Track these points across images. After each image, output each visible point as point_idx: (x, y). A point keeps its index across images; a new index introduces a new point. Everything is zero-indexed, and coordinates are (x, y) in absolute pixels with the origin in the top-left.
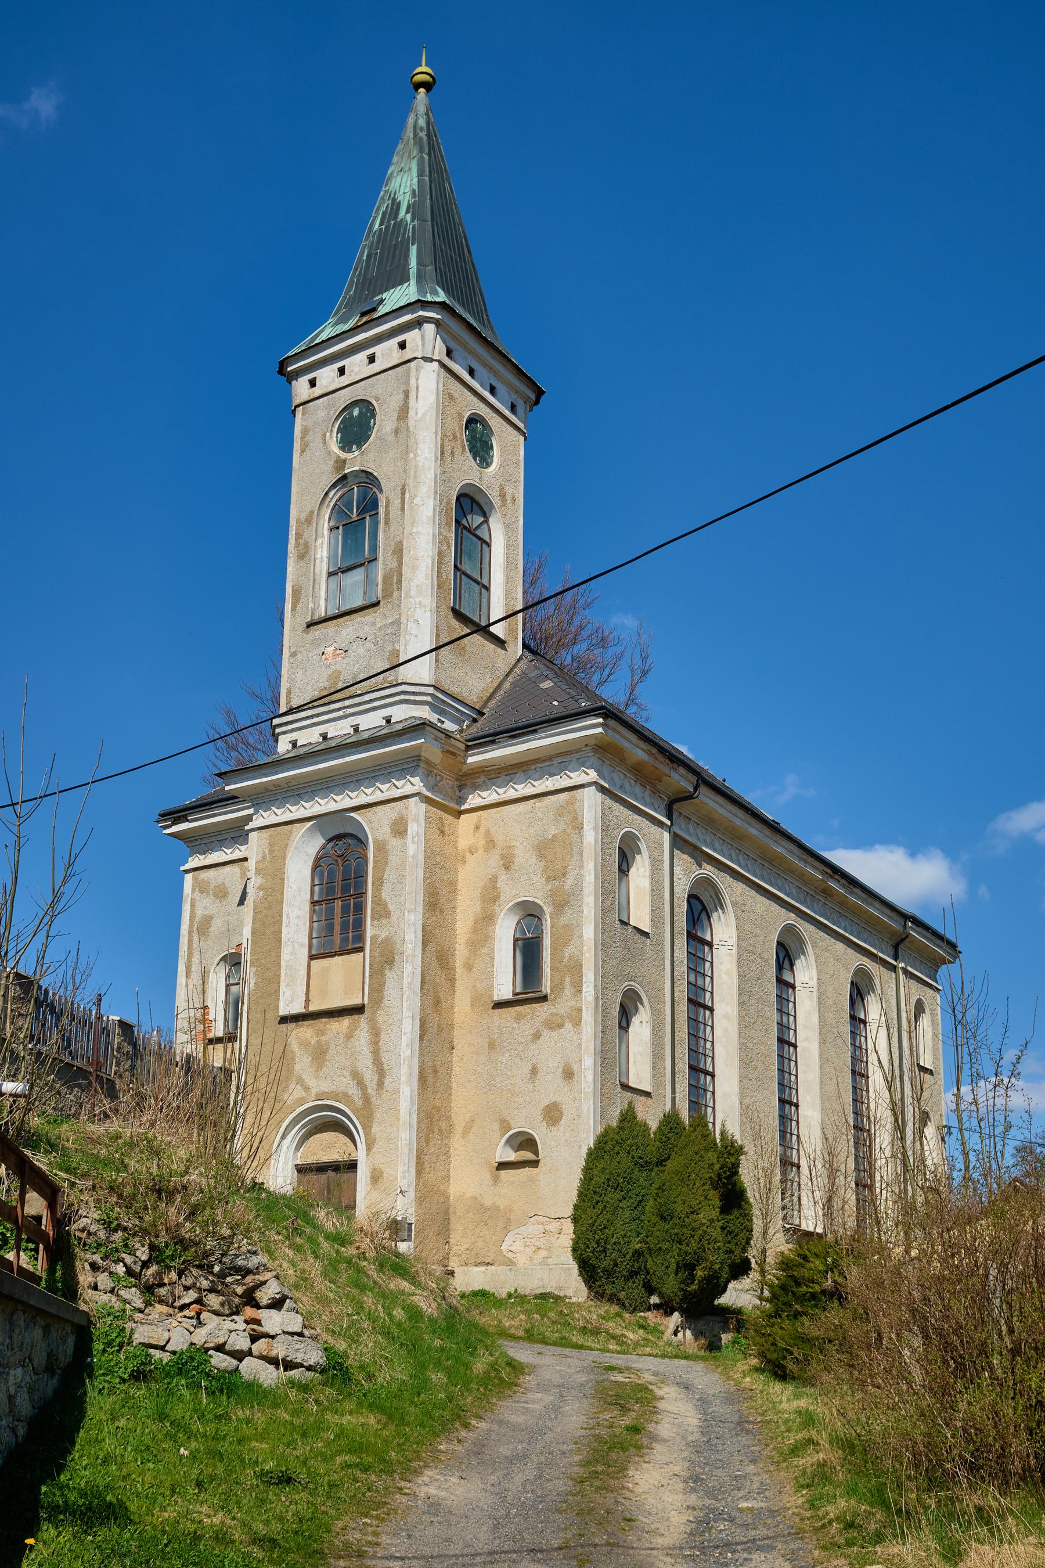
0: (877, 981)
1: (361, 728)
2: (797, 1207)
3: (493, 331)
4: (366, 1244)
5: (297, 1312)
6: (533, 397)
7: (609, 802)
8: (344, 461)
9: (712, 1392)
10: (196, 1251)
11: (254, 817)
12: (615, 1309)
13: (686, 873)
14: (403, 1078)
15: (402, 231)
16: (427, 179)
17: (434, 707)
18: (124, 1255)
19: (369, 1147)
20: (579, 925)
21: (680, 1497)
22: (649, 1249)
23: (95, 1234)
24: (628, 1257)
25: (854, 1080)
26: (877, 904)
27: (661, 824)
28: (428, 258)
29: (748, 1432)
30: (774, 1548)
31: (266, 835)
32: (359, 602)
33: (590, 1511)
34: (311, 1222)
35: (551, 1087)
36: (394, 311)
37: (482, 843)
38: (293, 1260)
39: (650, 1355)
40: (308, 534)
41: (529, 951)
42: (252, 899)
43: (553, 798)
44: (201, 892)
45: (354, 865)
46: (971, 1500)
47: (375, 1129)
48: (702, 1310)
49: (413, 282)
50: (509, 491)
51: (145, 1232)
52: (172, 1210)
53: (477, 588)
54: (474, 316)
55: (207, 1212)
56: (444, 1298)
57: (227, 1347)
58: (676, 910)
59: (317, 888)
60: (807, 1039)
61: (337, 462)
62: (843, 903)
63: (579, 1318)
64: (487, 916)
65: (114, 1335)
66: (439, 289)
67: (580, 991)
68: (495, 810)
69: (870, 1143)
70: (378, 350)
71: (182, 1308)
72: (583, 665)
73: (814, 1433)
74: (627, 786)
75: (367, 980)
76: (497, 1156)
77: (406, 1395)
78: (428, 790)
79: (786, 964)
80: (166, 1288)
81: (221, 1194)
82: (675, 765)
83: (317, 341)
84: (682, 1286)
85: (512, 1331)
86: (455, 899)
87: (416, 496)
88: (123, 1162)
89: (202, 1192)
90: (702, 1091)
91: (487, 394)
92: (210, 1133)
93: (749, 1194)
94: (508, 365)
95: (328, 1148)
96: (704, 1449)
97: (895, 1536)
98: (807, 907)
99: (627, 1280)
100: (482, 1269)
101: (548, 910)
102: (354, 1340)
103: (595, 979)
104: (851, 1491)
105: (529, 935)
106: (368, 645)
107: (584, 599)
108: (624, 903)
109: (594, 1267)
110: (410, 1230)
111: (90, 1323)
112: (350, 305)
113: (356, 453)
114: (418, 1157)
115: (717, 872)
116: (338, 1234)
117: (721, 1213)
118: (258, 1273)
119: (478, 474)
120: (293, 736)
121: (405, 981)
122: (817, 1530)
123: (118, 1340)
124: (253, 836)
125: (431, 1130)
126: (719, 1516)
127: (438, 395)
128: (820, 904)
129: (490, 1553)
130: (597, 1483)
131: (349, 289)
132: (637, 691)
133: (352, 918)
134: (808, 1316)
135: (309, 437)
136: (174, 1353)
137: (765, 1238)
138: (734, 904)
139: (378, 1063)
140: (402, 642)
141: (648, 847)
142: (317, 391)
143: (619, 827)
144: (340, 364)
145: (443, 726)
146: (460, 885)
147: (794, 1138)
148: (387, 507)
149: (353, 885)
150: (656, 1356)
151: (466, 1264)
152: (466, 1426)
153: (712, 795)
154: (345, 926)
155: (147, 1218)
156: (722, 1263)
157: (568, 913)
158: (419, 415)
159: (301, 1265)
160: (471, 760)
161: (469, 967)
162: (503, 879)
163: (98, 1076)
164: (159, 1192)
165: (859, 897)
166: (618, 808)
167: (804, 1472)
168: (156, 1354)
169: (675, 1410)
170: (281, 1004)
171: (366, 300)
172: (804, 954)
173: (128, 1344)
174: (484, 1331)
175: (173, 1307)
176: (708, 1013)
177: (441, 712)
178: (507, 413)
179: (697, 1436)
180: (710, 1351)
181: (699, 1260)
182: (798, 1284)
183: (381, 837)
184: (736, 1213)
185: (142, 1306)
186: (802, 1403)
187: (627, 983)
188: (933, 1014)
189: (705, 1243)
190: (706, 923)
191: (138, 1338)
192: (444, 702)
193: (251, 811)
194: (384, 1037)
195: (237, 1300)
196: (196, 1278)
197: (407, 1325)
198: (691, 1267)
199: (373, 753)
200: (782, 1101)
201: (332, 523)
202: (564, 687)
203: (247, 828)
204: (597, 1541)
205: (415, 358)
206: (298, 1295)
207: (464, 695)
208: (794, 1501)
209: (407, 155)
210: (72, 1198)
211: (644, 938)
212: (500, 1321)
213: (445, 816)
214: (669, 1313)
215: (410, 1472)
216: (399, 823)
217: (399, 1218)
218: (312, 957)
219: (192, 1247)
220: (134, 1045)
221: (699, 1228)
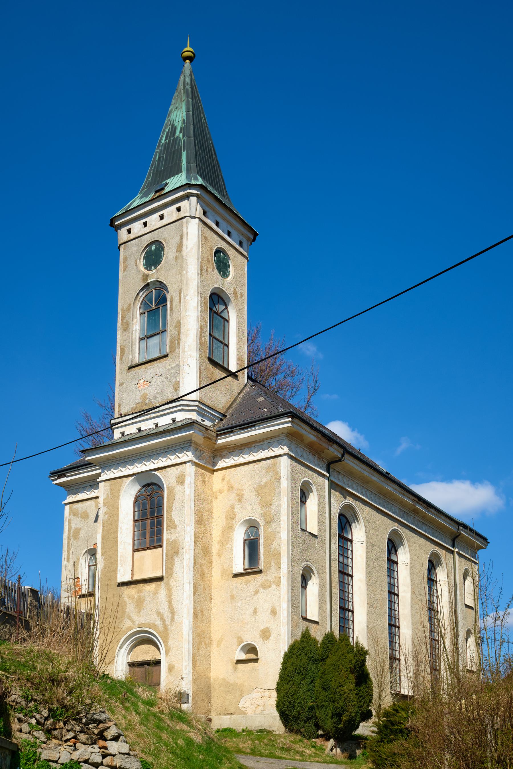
0: (443, 559)
1: (159, 425)
2: (396, 682)
3: (229, 201)
4: (164, 706)
5: (126, 743)
6: (252, 237)
7: (295, 464)
8: (147, 276)
10: (73, 712)
11: (102, 474)
12: (299, 737)
13: (338, 502)
15: (177, 143)
16: (191, 113)
17: (199, 413)
18: (35, 714)
19: (167, 652)
22: (317, 706)
23: (20, 703)
24: (306, 710)
26: (443, 517)
28: (193, 159)
32: (157, 355)
34: (133, 694)
35: (264, 620)
36: (173, 190)
37: (226, 487)
38: (124, 715)
39: (317, 762)
40: (128, 317)
41: (252, 546)
42: (101, 519)
43: (264, 462)
44: (74, 515)
47: (170, 643)
49: (184, 173)
50: (239, 291)
51: (46, 702)
52: (60, 691)
53: (222, 345)
54: (218, 191)
55: (78, 692)
56: (206, 733)
57: (90, 761)
58: (332, 523)
61: (143, 276)
62: (424, 517)
63: (280, 743)
64: (229, 528)
65: (31, 755)
66: (199, 177)
67: (280, 568)
68: (233, 469)
69: (439, 646)
70: (165, 212)
71: (66, 741)
72: (281, 387)
74: (305, 455)
75: (164, 563)
78: (196, 459)
79: (393, 551)
80: (57, 731)
81: (85, 682)
82: (331, 443)
83: (131, 207)
84: (335, 725)
85: (244, 750)
87: (187, 295)
88: (33, 665)
89: (75, 681)
90: (347, 621)
91: (226, 236)
92: (79, 648)
93: (371, 676)
94: (238, 220)
95: (145, 653)
98: (405, 520)
99: (305, 722)
100: (229, 717)
101: (262, 524)
102: (156, 756)
103: (288, 561)
105: (252, 537)
106: (162, 378)
109: (288, 715)
110: (188, 698)
111: (18, 749)
112: (149, 186)
113: (154, 271)
115: (354, 501)
116: (149, 700)
117: (356, 686)
118: (106, 723)
119: (221, 282)
121: (185, 563)
123: (33, 758)
124: (101, 484)
127: (198, 237)
128: (412, 517)
131: (148, 178)
132: (311, 401)
133: (156, 529)
135: (128, 262)
136: (62, 764)
137: (380, 699)
140: (181, 377)
141: (317, 488)
142: (132, 236)
143: (300, 477)
144: (144, 220)
145: (204, 423)
146: (214, 510)
147: (397, 645)
148: (171, 301)
149: (156, 511)
150: (320, 762)
151: (220, 714)
154: (152, 534)
155: (47, 695)
156: (356, 713)
157: (273, 526)
158: (189, 249)
159: (129, 717)
160: (219, 442)
161: (219, 555)
162: (237, 507)
163: (20, 618)
164: (53, 681)
165: (433, 514)
166: (300, 467)
168: (53, 765)
170: (119, 576)
171: (158, 183)
172: (403, 545)
173: (38, 760)
174: (227, 750)
175: (61, 740)
176: (350, 578)
177: (203, 415)
178: (238, 247)
180: (350, 759)
181: (344, 711)
182: (393, 725)
183: (171, 485)
184: (364, 686)
185: (45, 740)
187: (305, 563)
189: (347, 702)
190: (349, 529)
191: (43, 757)
192: (204, 410)
193: (100, 471)
194: (174, 593)
195: (95, 737)
196: (73, 725)
197: (185, 748)
198: (339, 715)
201: (142, 311)
202: (270, 401)
203: (98, 480)
205: (186, 217)
206: (126, 733)
207: (215, 406)
209: (179, 99)
210: (7, 685)
211: (314, 538)
212: (238, 745)
213: (206, 473)
214: (328, 739)
216: (181, 477)
217: (183, 691)
218: (135, 551)
219: (71, 709)
220: (39, 602)
221: (344, 694)
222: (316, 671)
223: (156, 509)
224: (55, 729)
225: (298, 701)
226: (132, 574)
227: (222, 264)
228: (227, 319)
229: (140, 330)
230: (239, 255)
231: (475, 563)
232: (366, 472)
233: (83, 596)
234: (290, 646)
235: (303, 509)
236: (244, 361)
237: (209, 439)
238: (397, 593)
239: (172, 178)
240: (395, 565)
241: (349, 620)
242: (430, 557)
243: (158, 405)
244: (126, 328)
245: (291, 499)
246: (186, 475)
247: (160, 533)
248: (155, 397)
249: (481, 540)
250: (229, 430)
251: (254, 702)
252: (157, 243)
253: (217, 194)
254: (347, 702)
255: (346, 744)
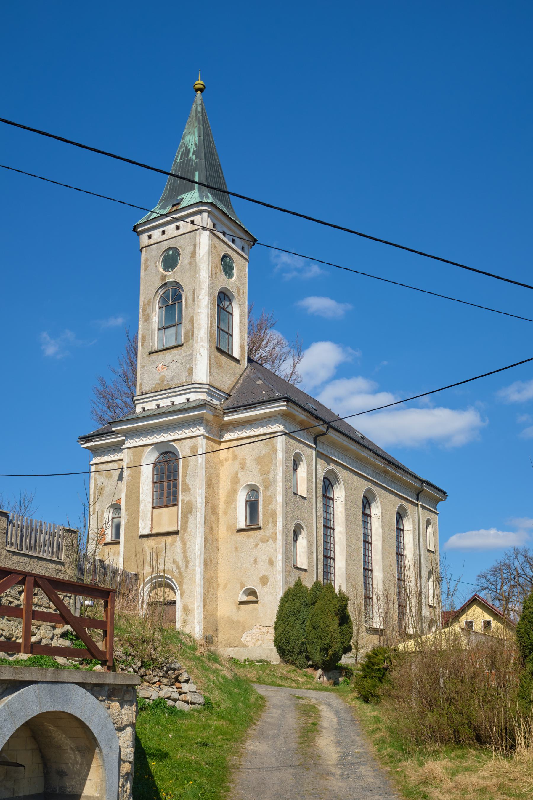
0: (409, 511)
8: (166, 276)
9: (340, 708)
11: (126, 442)
12: (293, 667)
13: (323, 468)
14: (197, 564)
15: (191, 164)
16: (202, 138)
17: (209, 394)
19: (182, 595)
20: (276, 496)
21: (334, 748)
22: (308, 642)
25: (398, 558)
26: (409, 476)
27: (311, 447)
29: (355, 724)
30: (367, 764)
31: (132, 451)
32: (173, 344)
33: (306, 754)
35: (263, 569)
36: (188, 206)
37: (231, 456)
41: (253, 507)
45: (172, 466)
46: (431, 749)
47: (184, 587)
48: (331, 667)
50: (241, 289)
53: (227, 335)
58: (318, 486)
59: (155, 476)
60: (376, 540)
62: (393, 476)
66: (209, 195)
67: (276, 526)
71: (153, 683)
73: (380, 726)
75: (180, 519)
76: (239, 598)
77: (232, 713)
78: (207, 433)
79: (367, 506)
82: (318, 421)
85: (251, 679)
86: (219, 482)
87: (199, 295)
91: (231, 244)
93: (352, 618)
94: (241, 229)
96: (340, 730)
97: (405, 760)
98: (377, 479)
99: (298, 655)
101: (261, 488)
104: (392, 746)
105: (253, 499)
106: (178, 364)
107: (270, 323)
108: (295, 484)
109: (284, 649)
112: (167, 198)
113: (171, 273)
114: (204, 599)
115: (336, 466)
117: (340, 626)
120: (143, 405)
121: (198, 520)
122: (381, 758)
125: (209, 587)
126: (348, 755)
127: (209, 246)
129: (277, 767)
130: (306, 744)
133: (172, 490)
134: (377, 678)
135: (149, 263)
136: (153, 700)
137: (358, 635)
138: (344, 481)
139: (185, 557)
140: (194, 364)
142: (152, 241)
143: (293, 450)
144: (163, 229)
145: (213, 402)
146: (221, 475)
147: (370, 585)
148: (186, 299)
152: (255, 724)
153: (334, 432)
154: (169, 494)
158: (201, 256)
160: (226, 419)
162: (241, 474)
165: (400, 474)
166: (293, 442)
167: (376, 740)
169: (327, 716)
171: (174, 197)
172: (375, 501)
178: (240, 252)
179: (337, 726)
181: (330, 647)
182: (373, 665)
184: (345, 625)
186: (375, 713)
188: (435, 525)
190: (331, 490)
192: (213, 391)
193: (124, 438)
194: (188, 545)
195: (173, 680)
198: (326, 650)
199: (182, 416)
200: (365, 569)
201: (160, 305)
202: (268, 384)
203: (122, 447)
204: (310, 763)
208: (373, 749)
214: (317, 669)
215: (243, 742)
216: (192, 442)
218: (154, 508)
222: (307, 613)
223: (172, 473)
224: (146, 675)
225: (292, 638)
226: (152, 528)
227: (227, 267)
228: (231, 312)
229: (158, 322)
230: (241, 259)
231: (436, 513)
232: (346, 442)
233: (106, 544)
234: (285, 592)
235: (295, 475)
236: (245, 348)
237: (218, 416)
238: (370, 541)
239: (187, 194)
240: (369, 518)
241: (331, 566)
242: (398, 510)
243: (174, 386)
244: (147, 319)
245: (286, 468)
246: (199, 446)
247: (176, 493)
248: (172, 380)
249: (441, 493)
250: (235, 409)
251: (256, 639)
252: (173, 249)
253: (224, 209)
254: (332, 639)
255: (331, 673)
